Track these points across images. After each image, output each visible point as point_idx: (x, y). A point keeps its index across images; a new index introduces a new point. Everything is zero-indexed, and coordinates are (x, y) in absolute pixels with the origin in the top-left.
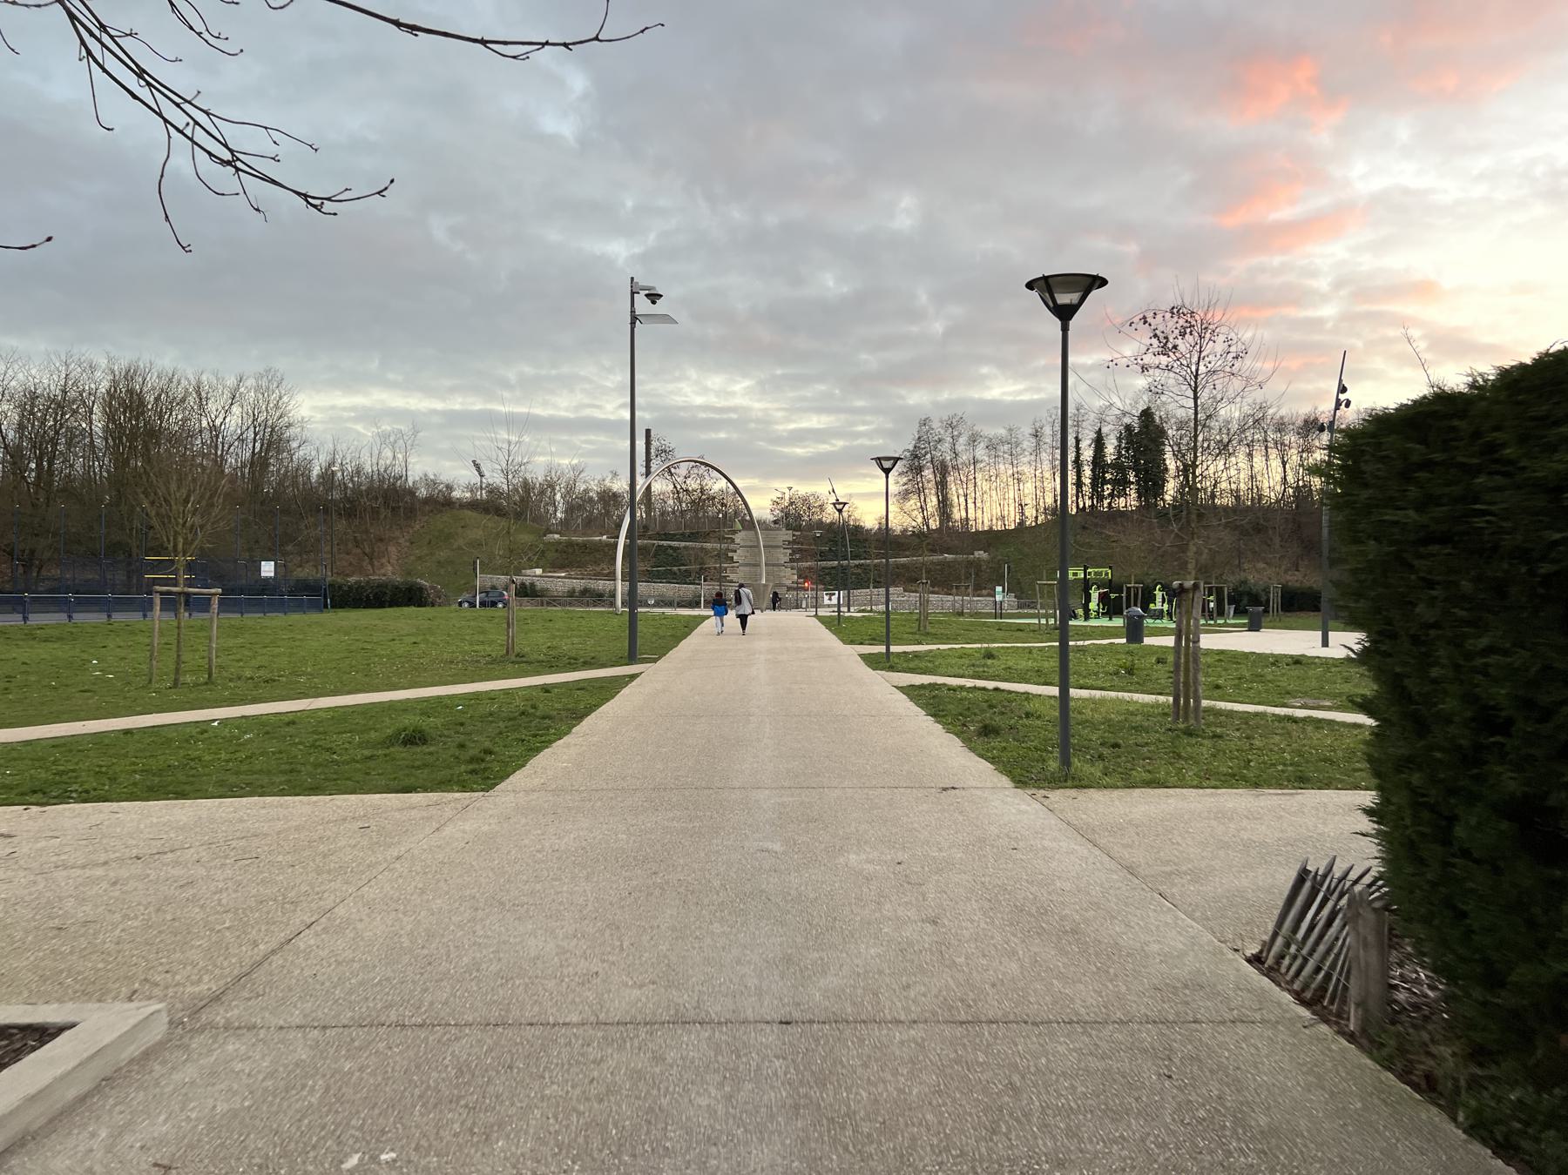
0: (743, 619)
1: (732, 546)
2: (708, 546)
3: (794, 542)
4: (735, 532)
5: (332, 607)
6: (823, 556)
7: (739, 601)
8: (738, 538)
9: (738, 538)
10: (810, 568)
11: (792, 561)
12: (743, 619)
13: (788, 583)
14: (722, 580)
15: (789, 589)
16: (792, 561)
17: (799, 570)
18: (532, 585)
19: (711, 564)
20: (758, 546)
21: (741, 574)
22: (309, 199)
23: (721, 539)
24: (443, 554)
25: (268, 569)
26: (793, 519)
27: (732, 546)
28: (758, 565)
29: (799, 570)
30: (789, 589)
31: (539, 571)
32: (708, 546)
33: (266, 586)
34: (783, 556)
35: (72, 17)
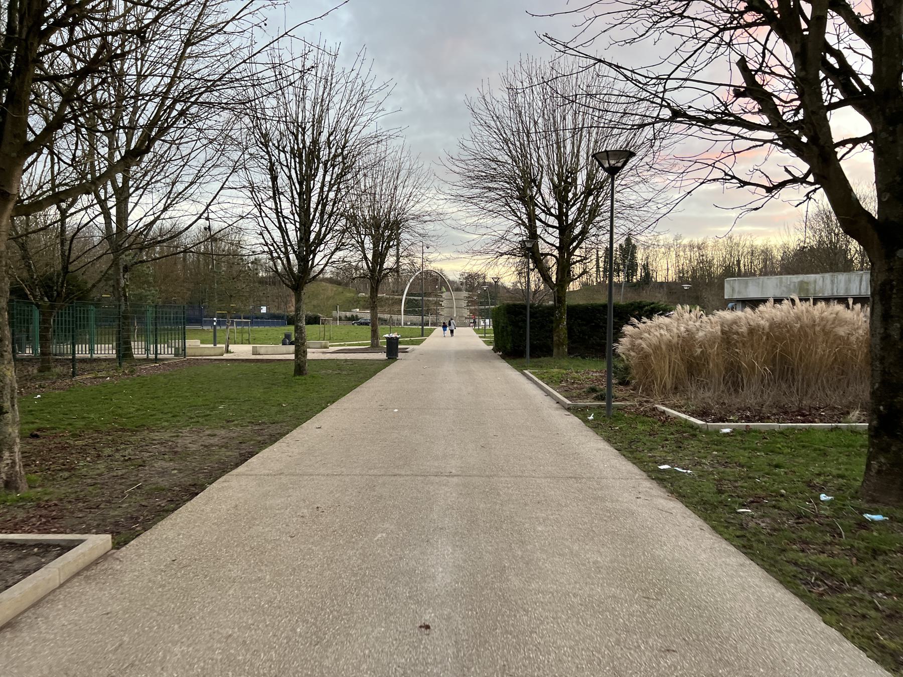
0: (452, 331)
1: (441, 299)
2: (431, 299)
3: (469, 297)
4: (442, 293)
5: (531, 356)
6: (482, 304)
7: (450, 324)
8: (444, 295)
9: (444, 295)
10: (475, 309)
11: (468, 306)
12: (452, 331)
13: (466, 316)
14: (437, 314)
15: (466, 318)
16: (468, 306)
17: (470, 310)
18: (357, 316)
19: (432, 307)
20: (452, 299)
21: (445, 312)
22: (237, 18)
23: (436, 296)
24: (315, 302)
25: (264, 310)
26: (471, 282)
27: (441, 299)
28: (452, 308)
29: (470, 310)
30: (466, 318)
31: (358, 310)
32: (431, 299)
33: (263, 316)
34: (464, 303)
35: (141, 219)
